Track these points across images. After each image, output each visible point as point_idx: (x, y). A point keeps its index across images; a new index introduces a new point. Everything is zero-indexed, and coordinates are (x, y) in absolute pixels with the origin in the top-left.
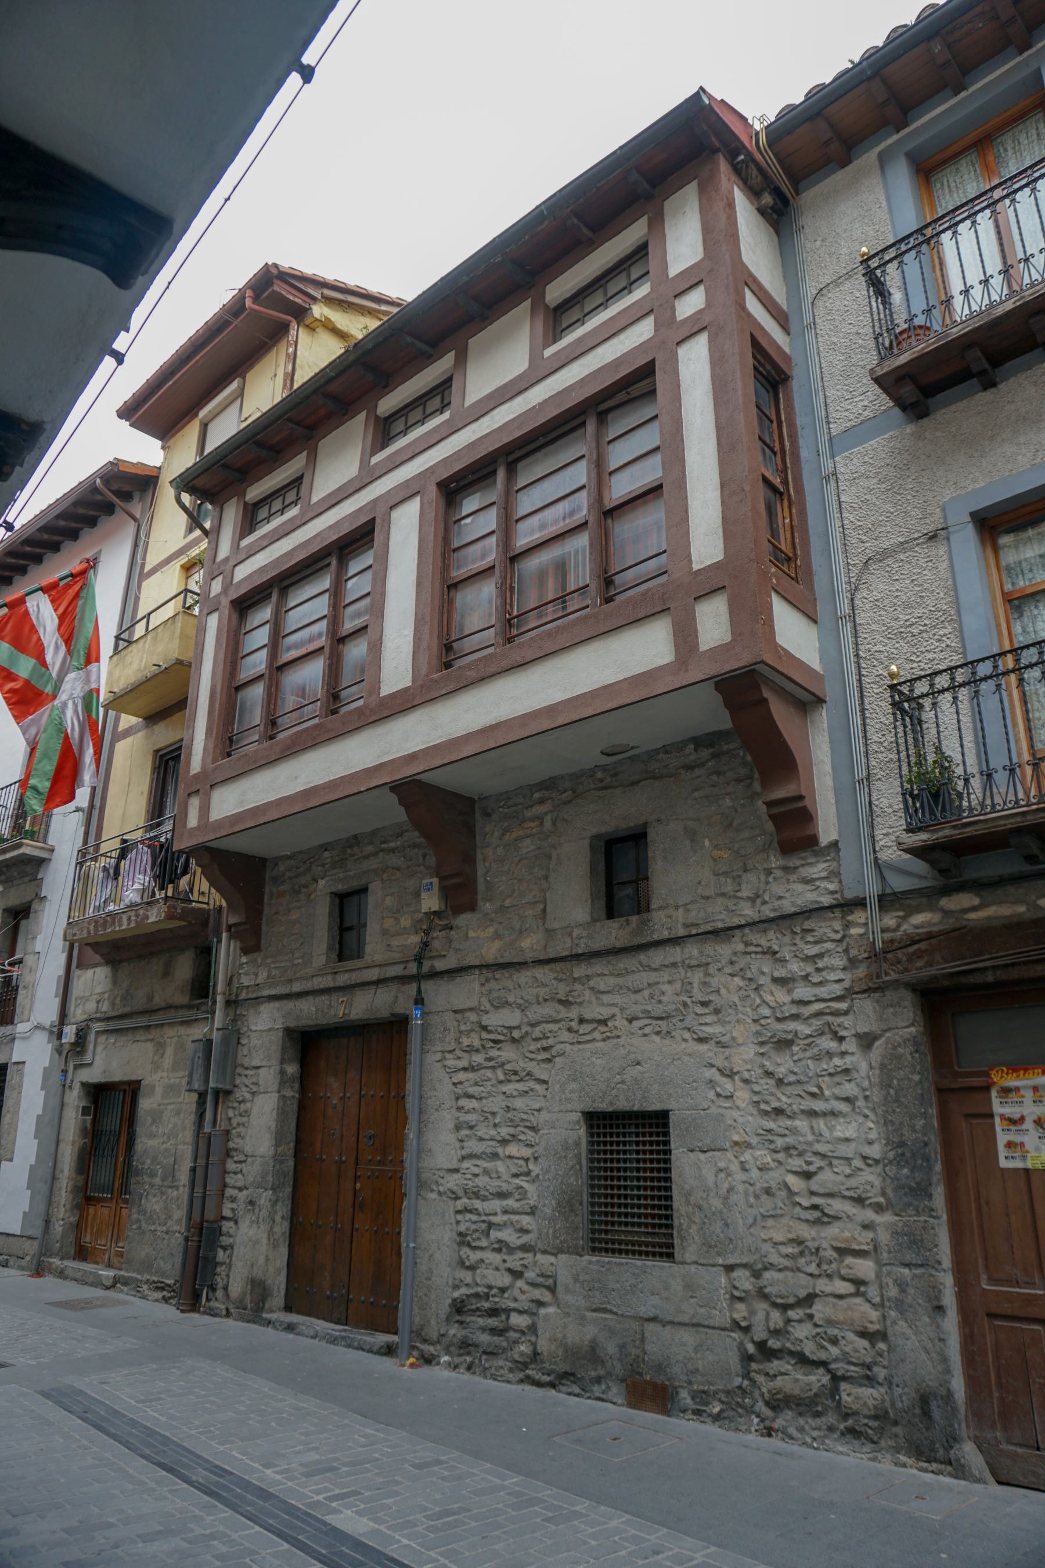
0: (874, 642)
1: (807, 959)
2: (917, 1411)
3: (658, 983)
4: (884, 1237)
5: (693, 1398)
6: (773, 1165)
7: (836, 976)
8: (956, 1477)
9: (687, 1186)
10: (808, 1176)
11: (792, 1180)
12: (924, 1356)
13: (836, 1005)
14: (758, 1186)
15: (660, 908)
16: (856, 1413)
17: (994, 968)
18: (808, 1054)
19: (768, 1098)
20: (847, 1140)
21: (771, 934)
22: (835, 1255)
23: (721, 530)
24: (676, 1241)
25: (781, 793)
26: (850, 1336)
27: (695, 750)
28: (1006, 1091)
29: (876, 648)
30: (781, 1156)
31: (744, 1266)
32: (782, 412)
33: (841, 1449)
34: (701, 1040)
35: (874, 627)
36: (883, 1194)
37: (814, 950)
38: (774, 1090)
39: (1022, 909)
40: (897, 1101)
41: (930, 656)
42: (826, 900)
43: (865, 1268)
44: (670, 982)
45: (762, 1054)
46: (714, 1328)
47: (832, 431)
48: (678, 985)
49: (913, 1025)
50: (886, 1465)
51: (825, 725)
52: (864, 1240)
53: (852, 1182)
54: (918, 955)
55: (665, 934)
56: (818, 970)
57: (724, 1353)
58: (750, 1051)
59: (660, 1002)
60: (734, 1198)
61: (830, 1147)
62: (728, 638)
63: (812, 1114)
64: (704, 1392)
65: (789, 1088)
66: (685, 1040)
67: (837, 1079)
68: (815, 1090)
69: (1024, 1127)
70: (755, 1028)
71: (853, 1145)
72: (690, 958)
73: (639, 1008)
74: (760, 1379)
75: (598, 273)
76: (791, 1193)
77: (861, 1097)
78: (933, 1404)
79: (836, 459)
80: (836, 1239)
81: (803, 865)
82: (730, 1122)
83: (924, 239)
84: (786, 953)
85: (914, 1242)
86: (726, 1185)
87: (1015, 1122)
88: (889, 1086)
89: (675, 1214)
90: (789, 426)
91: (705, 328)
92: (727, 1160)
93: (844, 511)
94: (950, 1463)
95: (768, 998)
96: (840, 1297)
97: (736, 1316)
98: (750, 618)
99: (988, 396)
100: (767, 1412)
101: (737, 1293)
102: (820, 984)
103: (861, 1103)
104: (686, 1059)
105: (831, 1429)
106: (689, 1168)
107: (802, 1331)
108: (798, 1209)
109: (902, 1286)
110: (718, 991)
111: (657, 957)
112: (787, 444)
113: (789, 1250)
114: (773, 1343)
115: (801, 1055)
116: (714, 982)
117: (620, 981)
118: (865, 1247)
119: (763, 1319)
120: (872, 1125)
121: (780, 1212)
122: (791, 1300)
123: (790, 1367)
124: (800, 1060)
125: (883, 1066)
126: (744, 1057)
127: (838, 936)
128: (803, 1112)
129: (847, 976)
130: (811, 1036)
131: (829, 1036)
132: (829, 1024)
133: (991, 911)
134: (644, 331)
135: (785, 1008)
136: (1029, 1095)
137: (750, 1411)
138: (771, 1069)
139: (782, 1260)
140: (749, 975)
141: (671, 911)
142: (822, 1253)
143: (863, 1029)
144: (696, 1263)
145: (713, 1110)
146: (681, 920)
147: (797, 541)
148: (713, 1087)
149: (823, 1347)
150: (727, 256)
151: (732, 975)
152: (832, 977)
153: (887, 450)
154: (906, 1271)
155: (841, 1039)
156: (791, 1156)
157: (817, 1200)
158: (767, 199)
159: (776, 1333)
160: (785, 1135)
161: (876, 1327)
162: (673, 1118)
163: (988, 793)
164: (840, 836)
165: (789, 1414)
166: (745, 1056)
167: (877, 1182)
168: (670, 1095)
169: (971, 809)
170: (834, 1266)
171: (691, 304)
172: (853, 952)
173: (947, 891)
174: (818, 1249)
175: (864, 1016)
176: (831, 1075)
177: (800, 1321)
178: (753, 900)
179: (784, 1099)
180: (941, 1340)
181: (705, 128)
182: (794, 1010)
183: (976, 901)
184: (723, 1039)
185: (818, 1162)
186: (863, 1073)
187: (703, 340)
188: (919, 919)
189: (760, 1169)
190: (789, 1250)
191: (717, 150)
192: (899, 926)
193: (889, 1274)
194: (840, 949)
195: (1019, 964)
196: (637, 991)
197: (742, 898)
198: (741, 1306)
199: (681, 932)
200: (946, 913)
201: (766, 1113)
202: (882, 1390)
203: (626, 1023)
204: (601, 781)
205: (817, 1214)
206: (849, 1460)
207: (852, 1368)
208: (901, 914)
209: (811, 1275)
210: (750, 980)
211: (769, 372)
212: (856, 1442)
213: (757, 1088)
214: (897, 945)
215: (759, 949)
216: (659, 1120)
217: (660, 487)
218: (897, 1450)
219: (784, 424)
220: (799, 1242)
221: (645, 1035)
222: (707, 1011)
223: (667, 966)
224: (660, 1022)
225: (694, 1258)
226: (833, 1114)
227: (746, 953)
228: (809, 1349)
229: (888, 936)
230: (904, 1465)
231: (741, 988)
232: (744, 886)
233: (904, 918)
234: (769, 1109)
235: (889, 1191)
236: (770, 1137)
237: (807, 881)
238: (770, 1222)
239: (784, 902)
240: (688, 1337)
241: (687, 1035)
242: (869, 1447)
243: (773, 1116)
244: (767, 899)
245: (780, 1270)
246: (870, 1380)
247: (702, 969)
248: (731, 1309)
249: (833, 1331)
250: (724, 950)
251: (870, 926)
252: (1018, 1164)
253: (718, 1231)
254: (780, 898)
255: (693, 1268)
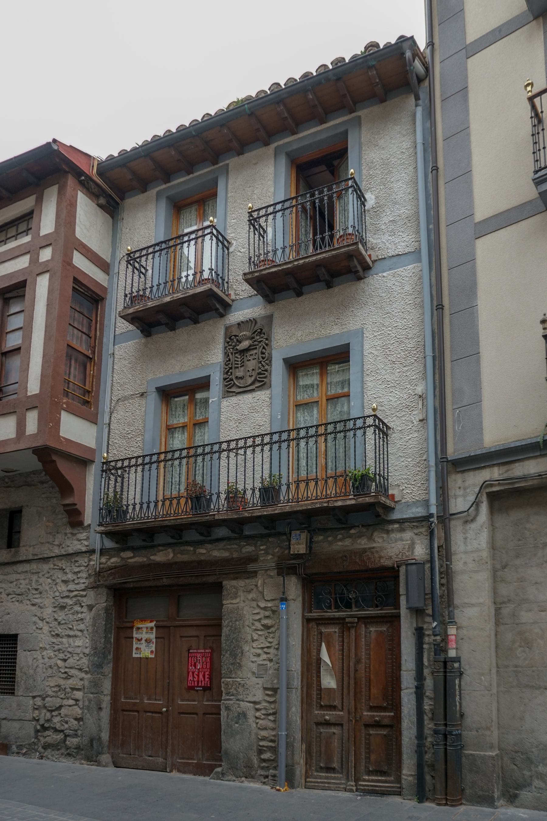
0: (116, 440)
1: (75, 573)
2: (89, 745)
3: (19, 579)
4: (86, 683)
5: (17, 748)
6: (53, 656)
7: (84, 581)
8: (97, 766)
9: (22, 665)
10: (65, 660)
11: (60, 663)
12: (94, 726)
13: (82, 593)
14: (47, 665)
15: (24, 546)
16: (70, 748)
17: (133, 582)
18: (70, 612)
19: (55, 629)
20: (79, 646)
21: (63, 562)
22: (70, 690)
23: (40, 378)
24: (16, 688)
25: (68, 501)
26: (72, 720)
27: (45, 475)
28: (138, 629)
29: (115, 441)
30: (56, 653)
31: (39, 696)
32: (99, 316)
33: (64, 761)
34: (33, 605)
35: (116, 431)
36: (88, 667)
37: (77, 570)
38: (57, 626)
39: (145, 560)
40: (97, 632)
41: (133, 449)
42: (84, 549)
43: (79, 695)
44: (24, 579)
45: (55, 612)
46: (26, 721)
47: (116, 332)
48: (27, 581)
49: (106, 602)
50: (77, 765)
51: (93, 473)
52: (80, 684)
53: (79, 663)
54: (111, 574)
55: (24, 558)
56: (78, 578)
57: (30, 728)
58: (49, 610)
59: (19, 588)
60: (38, 669)
61: (73, 649)
62: (36, 432)
63: (69, 636)
64: (21, 745)
65: (62, 626)
66: (27, 605)
67: (79, 622)
68: (71, 627)
69: (142, 642)
70: (53, 600)
71: (80, 648)
72: (33, 569)
73: (11, 590)
74: (41, 739)
75: (14, 218)
76: (59, 668)
77: (86, 630)
78: (94, 742)
79: (116, 347)
80: (71, 684)
81: (78, 533)
82: (40, 639)
83: (171, 245)
84: (67, 571)
85: (96, 685)
86: (36, 665)
87: (139, 640)
88: (95, 626)
89: (16, 676)
90: (100, 324)
91: (48, 271)
92: (37, 655)
93: (114, 373)
94: (96, 762)
95: (59, 588)
96: (70, 706)
97: (35, 715)
98: (49, 422)
99: (170, 334)
100: (43, 751)
101: (35, 707)
102: (78, 584)
103: (85, 632)
104: (27, 612)
105: (62, 754)
106: (24, 658)
107: (56, 720)
108: (60, 673)
109: (90, 701)
110: (41, 584)
111: (20, 568)
112: (98, 333)
113: (55, 689)
114: (47, 725)
115: (68, 613)
116: (41, 580)
117: (5, 577)
118: (80, 687)
119: (44, 715)
120: (88, 641)
121: (54, 675)
122: (54, 708)
123: (51, 733)
124: (67, 614)
125: (94, 618)
126: (48, 612)
127: (86, 565)
128: (66, 635)
129: (87, 581)
130: (72, 605)
131: (78, 605)
132: (78, 600)
133: (136, 559)
134: (23, 262)
135: (64, 593)
136: (145, 630)
137: (36, 751)
138: (57, 618)
139: (52, 693)
140: (53, 578)
141: (27, 548)
142: (66, 690)
143: (89, 603)
144: (22, 696)
145: (35, 634)
146: (31, 552)
147: (94, 383)
148: (35, 625)
149: (63, 725)
150: (63, 234)
151: (48, 578)
152: (82, 581)
153: (134, 348)
154: (92, 695)
155: (82, 606)
156: (60, 653)
157: (67, 670)
158: (102, 201)
159: (48, 721)
160: (58, 645)
161: (80, 716)
162: (19, 637)
163: (325, 489)
164: (92, 521)
165: (49, 750)
166: (48, 612)
167: (87, 663)
168: (19, 628)
169: (254, 504)
170: (69, 694)
171: (46, 255)
172: (90, 572)
173: (123, 550)
174: (65, 688)
175: (90, 598)
176: (77, 621)
177: (56, 716)
178: (59, 546)
179: (60, 630)
180: (99, 719)
181: (58, 160)
182: (67, 594)
183: (132, 555)
184: (41, 605)
185: (69, 655)
186: (87, 621)
187: (47, 276)
188: (113, 560)
189: (49, 658)
190: (55, 689)
191: (67, 172)
192: (107, 562)
193: (86, 697)
194: (86, 570)
195: (141, 581)
196: (11, 582)
197: (55, 545)
198: (37, 712)
199: (31, 557)
200: (123, 559)
201: (53, 636)
202: (79, 739)
203: (6, 596)
204: (7, 483)
205: (66, 675)
206: (66, 763)
207: (71, 732)
208: (108, 557)
209: (61, 698)
210: (54, 580)
211: (91, 295)
212: (69, 758)
213: (51, 625)
214: (104, 570)
215: (58, 567)
216: (14, 638)
217: (19, 349)
218: (82, 759)
219: (98, 322)
220: (59, 686)
221: (13, 602)
222: (37, 592)
223: (23, 572)
224: (19, 596)
225: (21, 694)
226: (76, 636)
227: (53, 569)
228: (58, 726)
229: (102, 566)
230: (83, 764)
231: (50, 584)
232: (56, 540)
233: (109, 559)
234: (54, 634)
235: (90, 666)
236: (54, 645)
237: (79, 540)
238: (50, 679)
239: (69, 548)
240: (17, 725)
241: (28, 602)
242: (73, 759)
243: (56, 637)
244: (63, 546)
245: (51, 697)
246: (76, 736)
247: (37, 575)
248: (33, 713)
249: (66, 719)
250: (45, 567)
251: (96, 560)
252: (138, 656)
253: (31, 683)
254: (68, 546)
255: (21, 698)
